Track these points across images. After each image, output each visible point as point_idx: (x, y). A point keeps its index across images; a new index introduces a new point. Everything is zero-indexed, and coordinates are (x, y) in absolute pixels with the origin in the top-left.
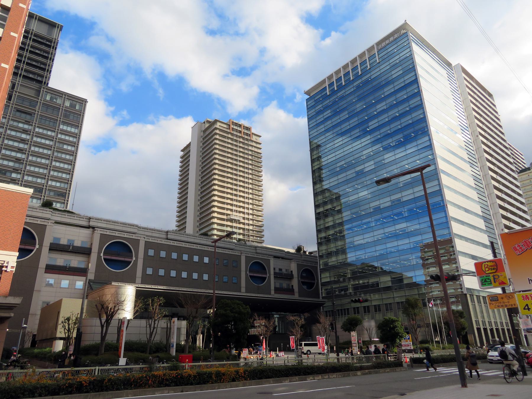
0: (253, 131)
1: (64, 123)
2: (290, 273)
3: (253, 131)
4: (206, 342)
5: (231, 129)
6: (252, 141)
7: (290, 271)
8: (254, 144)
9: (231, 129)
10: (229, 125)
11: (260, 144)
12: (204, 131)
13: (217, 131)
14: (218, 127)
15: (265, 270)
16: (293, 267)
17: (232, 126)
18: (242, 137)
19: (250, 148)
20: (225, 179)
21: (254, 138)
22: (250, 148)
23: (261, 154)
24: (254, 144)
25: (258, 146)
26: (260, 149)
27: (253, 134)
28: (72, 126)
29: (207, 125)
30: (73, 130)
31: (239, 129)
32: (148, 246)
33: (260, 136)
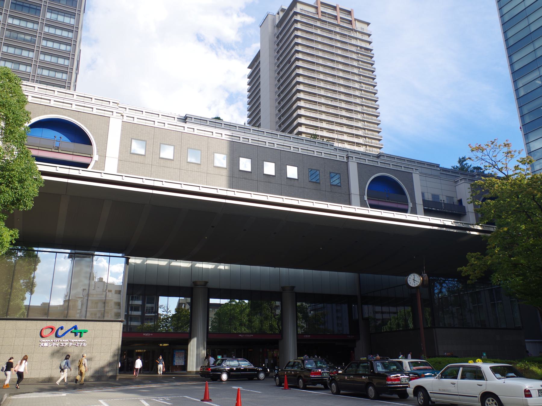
0: (356, 15)
1: (51, 10)
2: (456, 203)
3: (356, 15)
4: (138, 299)
5: (320, 13)
6: (356, 31)
7: (455, 201)
8: (359, 36)
9: (320, 13)
10: (316, 8)
11: (369, 35)
12: (278, 26)
13: (298, 18)
14: (298, 11)
15: (404, 194)
16: (464, 191)
17: (322, 9)
18: (338, 25)
19: (353, 42)
20: (316, 83)
21: (358, 26)
22: (353, 42)
23: (371, 50)
24: (359, 36)
25: (366, 38)
26: (370, 43)
27: (355, 20)
28: (65, 13)
29: (282, 14)
30: (67, 20)
31: (334, 13)
32: (131, 132)
33: (368, 24)
